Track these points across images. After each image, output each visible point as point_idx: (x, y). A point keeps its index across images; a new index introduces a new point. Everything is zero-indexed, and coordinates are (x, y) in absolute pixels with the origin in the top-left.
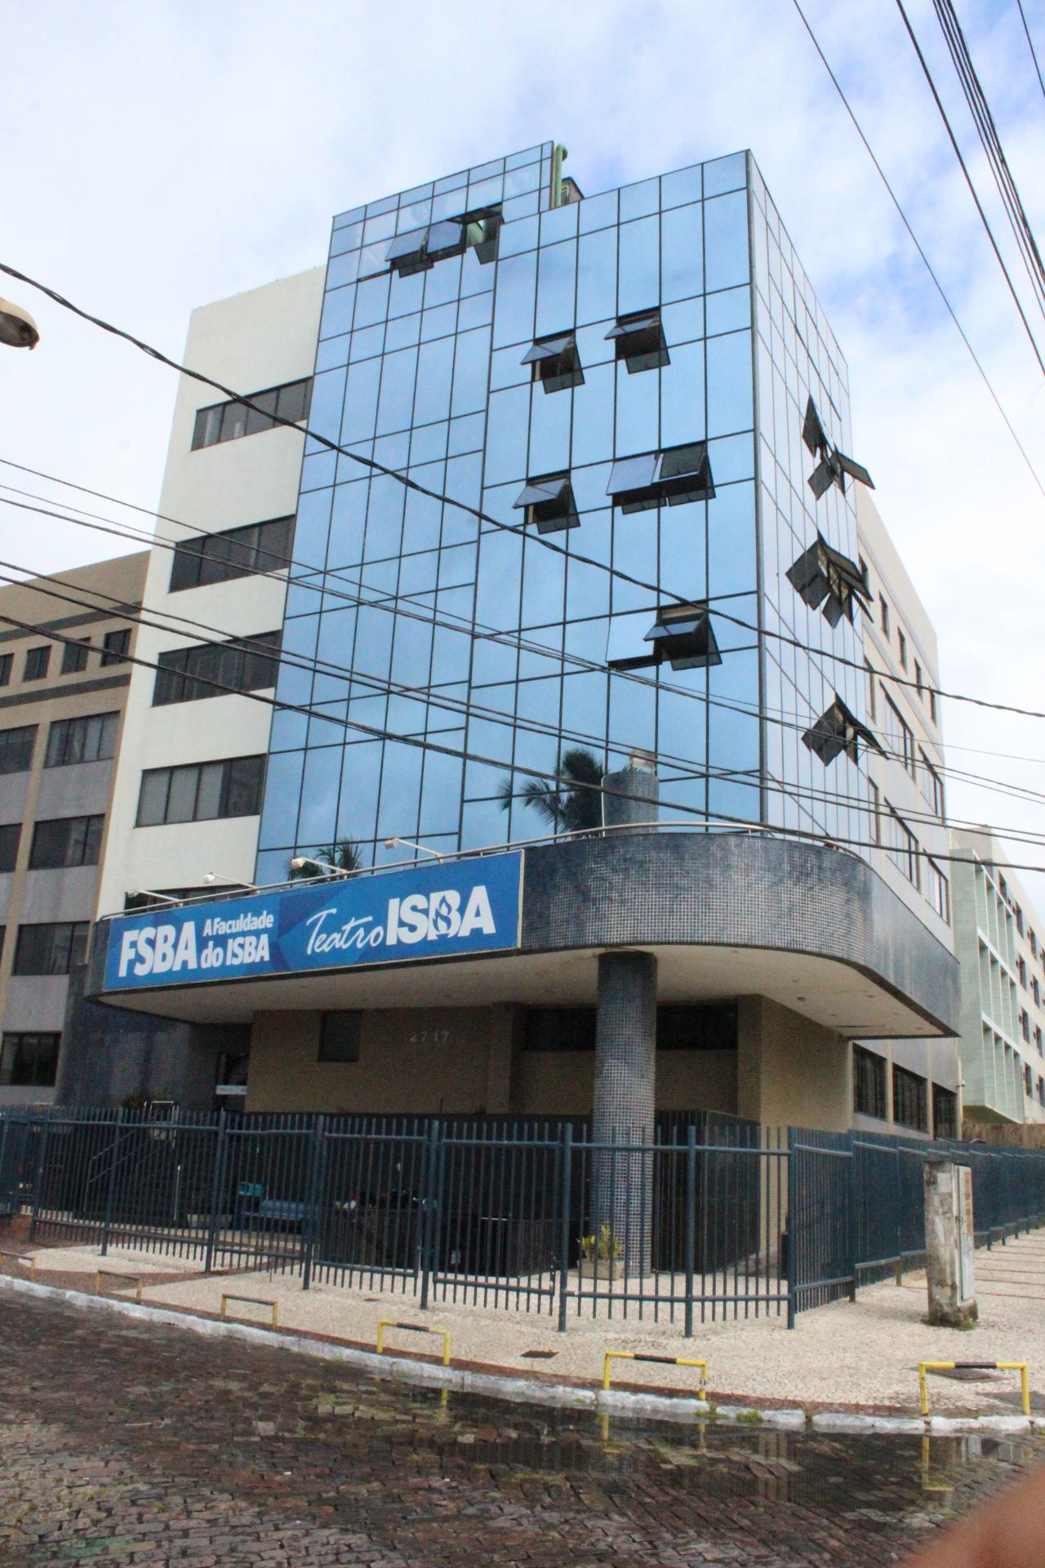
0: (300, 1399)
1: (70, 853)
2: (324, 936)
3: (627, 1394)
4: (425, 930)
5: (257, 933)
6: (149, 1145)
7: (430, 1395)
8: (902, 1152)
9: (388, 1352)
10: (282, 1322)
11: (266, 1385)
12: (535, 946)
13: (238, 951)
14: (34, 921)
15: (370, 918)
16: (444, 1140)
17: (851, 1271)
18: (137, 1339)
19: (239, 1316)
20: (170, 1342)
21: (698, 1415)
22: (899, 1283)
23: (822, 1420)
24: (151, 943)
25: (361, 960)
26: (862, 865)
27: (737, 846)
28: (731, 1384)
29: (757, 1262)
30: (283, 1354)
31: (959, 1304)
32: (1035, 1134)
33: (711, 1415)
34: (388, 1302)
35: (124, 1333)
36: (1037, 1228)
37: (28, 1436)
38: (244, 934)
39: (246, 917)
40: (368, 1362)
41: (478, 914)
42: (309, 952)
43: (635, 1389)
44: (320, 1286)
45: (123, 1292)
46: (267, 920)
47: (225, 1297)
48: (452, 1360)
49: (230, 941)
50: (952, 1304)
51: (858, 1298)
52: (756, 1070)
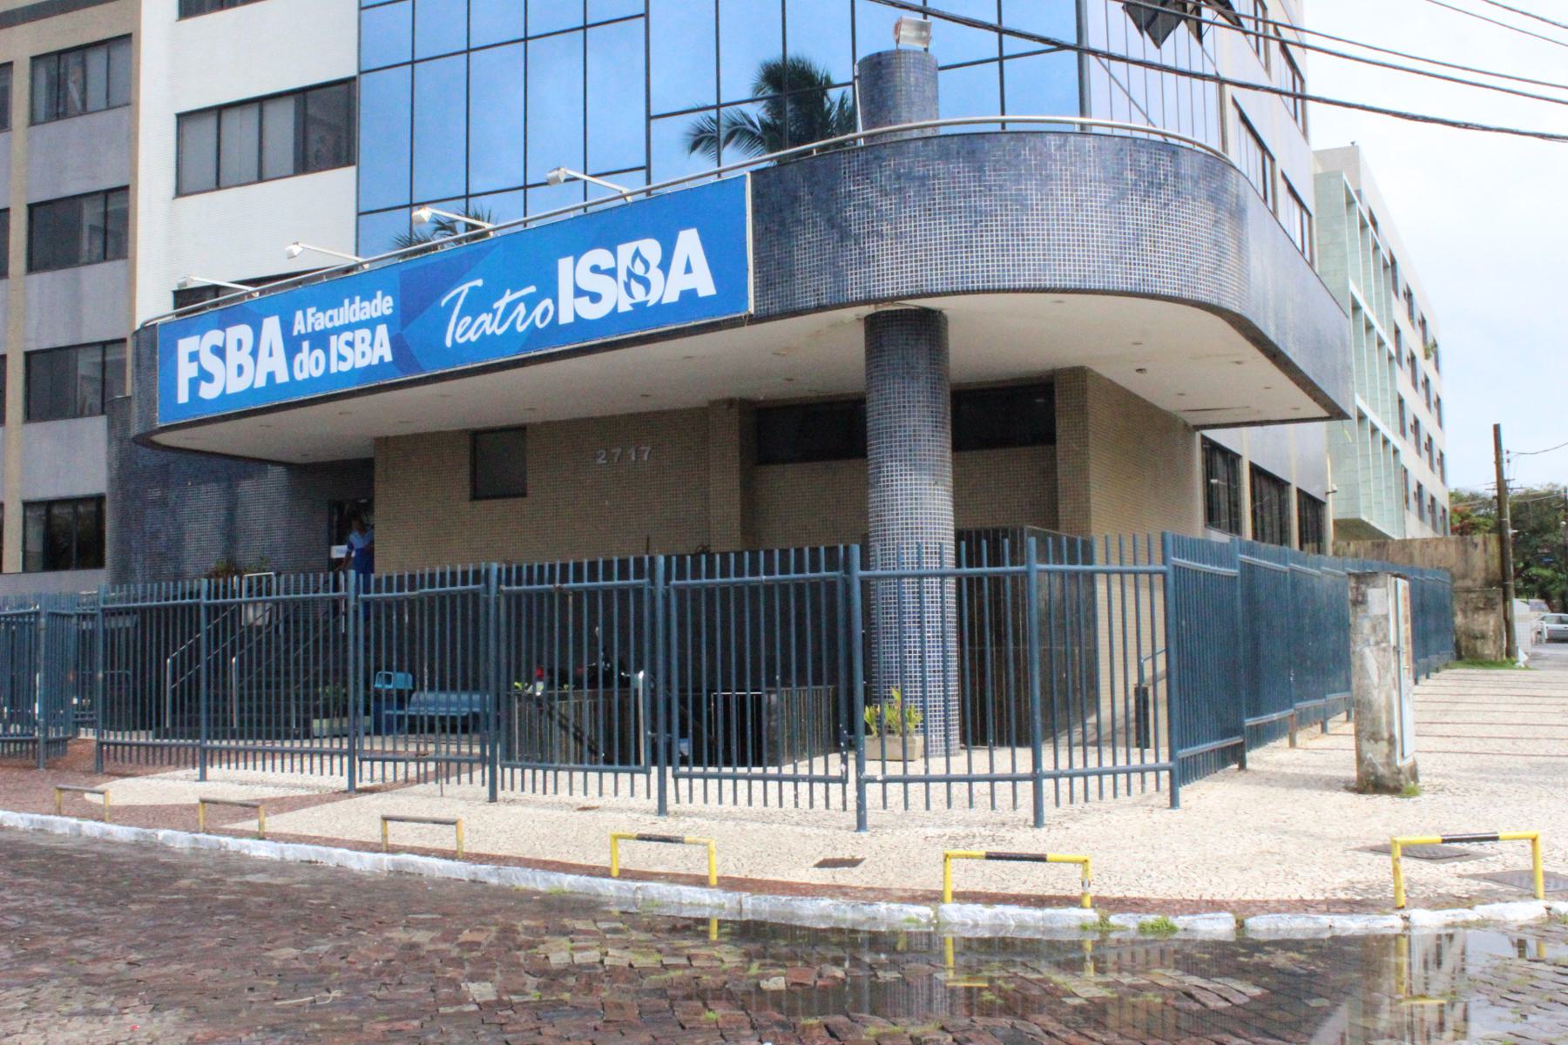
0: (519, 948)
1: (85, 245)
2: (468, 319)
3: (978, 907)
4: (615, 298)
5: (371, 324)
6: (242, 635)
7: (694, 927)
8: (1292, 570)
9: (625, 874)
10: (470, 846)
11: (467, 932)
12: (776, 308)
13: (346, 351)
14: (46, 345)
15: (532, 289)
16: (674, 582)
17: (1237, 730)
18: (269, 885)
19: (408, 844)
20: (317, 886)
21: (1084, 928)
22: (1293, 744)
23: (1260, 925)
24: (220, 352)
25: (524, 349)
26: (1234, 172)
27: (1059, 148)
28: (1119, 884)
29: (1098, 726)
30: (478, 888)
31: (1399, 763)
32: (1430, 551)
33: (1104, 927)
34: (610, 809)
35: (250, 878)
36: (1437, 671)
37: (133, 1029)
38: (351, 327)
39: (352, 302)
40: (601, 890)
41: (688, 270)
42: (449, 343)
43: (991, 899)
44: (512, 795)
45: (238, 826)
46: (383, 305)
47: (386, 819)
48: (719, 878)
49: (333, 339)
50: (1390, 762)
51: (1249, 765)
52: (1082, 473)
